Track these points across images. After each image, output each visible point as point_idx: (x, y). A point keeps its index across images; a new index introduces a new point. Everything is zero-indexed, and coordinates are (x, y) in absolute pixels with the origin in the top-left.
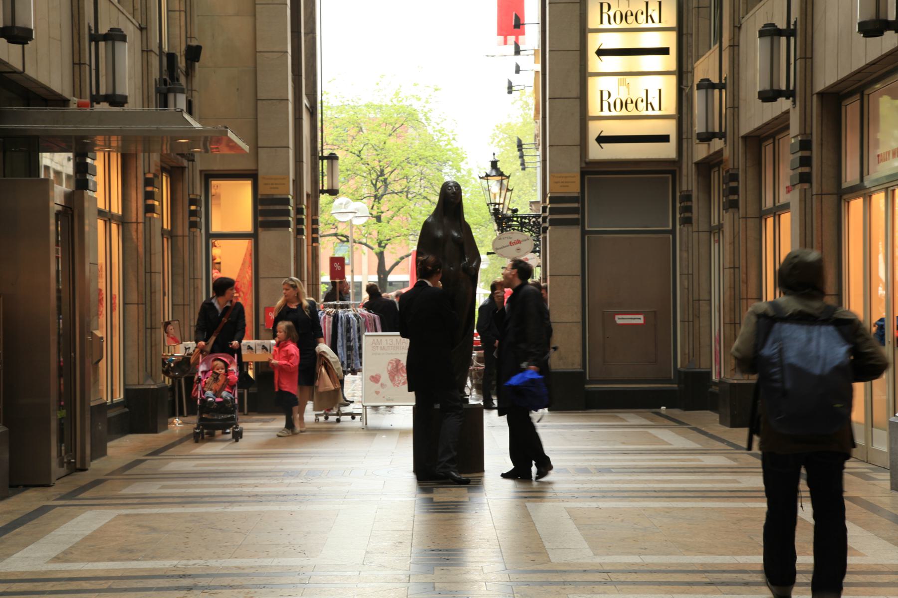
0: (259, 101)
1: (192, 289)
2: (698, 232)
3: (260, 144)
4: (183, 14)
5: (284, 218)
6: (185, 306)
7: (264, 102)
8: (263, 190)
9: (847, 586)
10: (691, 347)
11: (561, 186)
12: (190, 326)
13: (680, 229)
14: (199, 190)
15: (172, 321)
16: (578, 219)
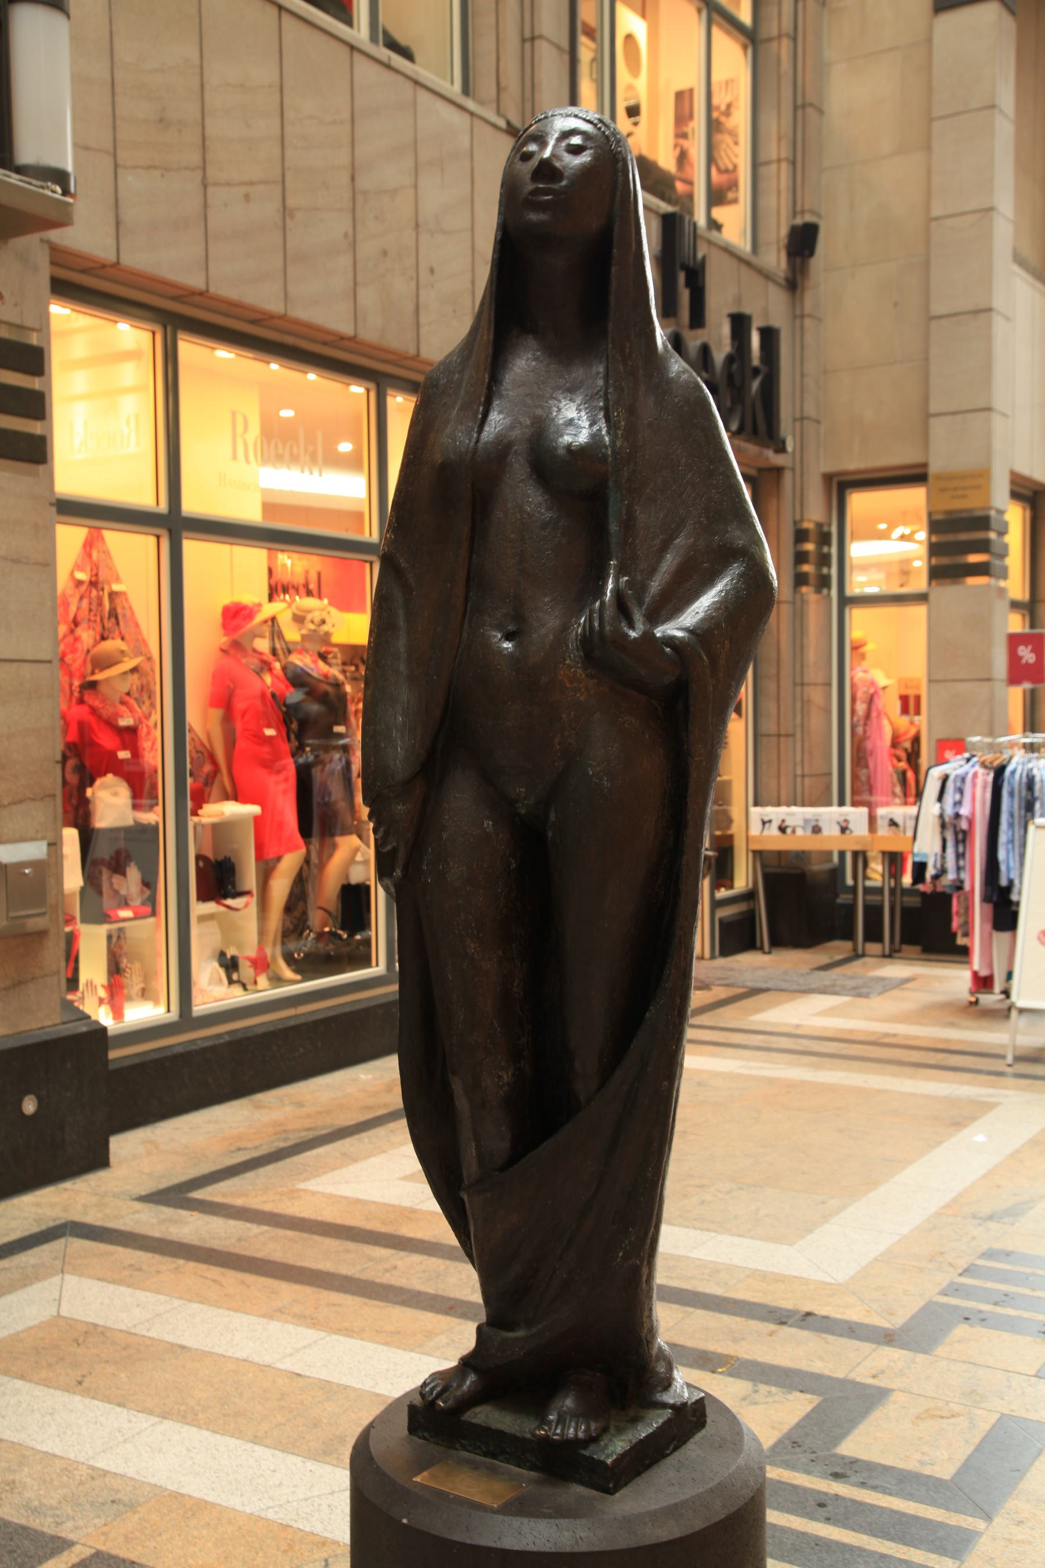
0: (934, 324)
1: (798, 705)
3: (933, 408)
4: (784, 166)
5: (979, 535)
6: (782, 739)
7: (943, 321)
12: (795, 776)
14: (815, 513)
15: (141, 654)
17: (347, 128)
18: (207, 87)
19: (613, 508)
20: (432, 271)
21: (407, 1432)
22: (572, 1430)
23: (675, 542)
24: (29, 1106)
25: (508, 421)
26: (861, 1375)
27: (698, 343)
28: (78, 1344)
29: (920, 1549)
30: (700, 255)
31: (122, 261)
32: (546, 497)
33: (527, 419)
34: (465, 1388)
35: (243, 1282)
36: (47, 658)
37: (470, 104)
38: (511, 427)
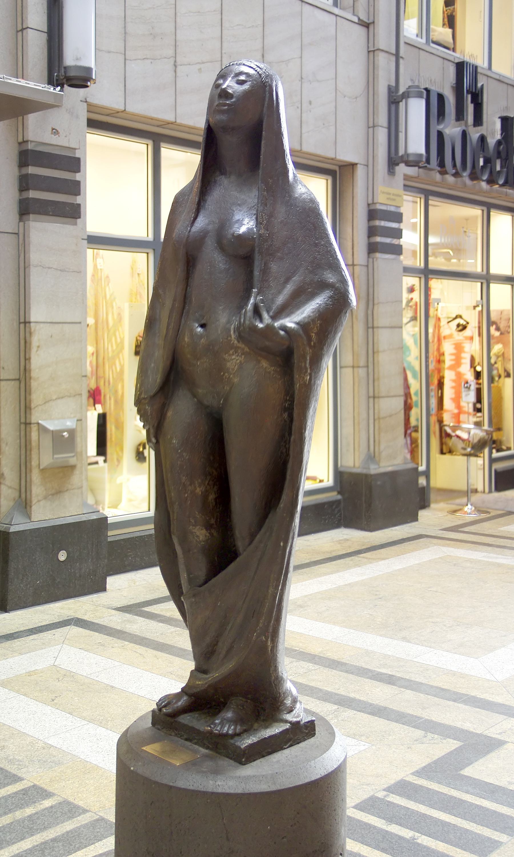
17: (261, 29)
18: (178, 14)
19: (257, 263)
20: (310, 103)
21: (151, 725)
22: (226, 729)
23: (293, 279)
24: (62, 556)
25: (207, 221)
26: (493, 733)
27: (478, 135)
28: (59, 681)
29: (490, 828)
30: (479, 85)
31: (126, 110)
32: (223, 258)
33: (217, 220)
34: (180, 703)
35: (156, 656)
36: (78, 321)
37: (336, 11)
38: (208, 225)
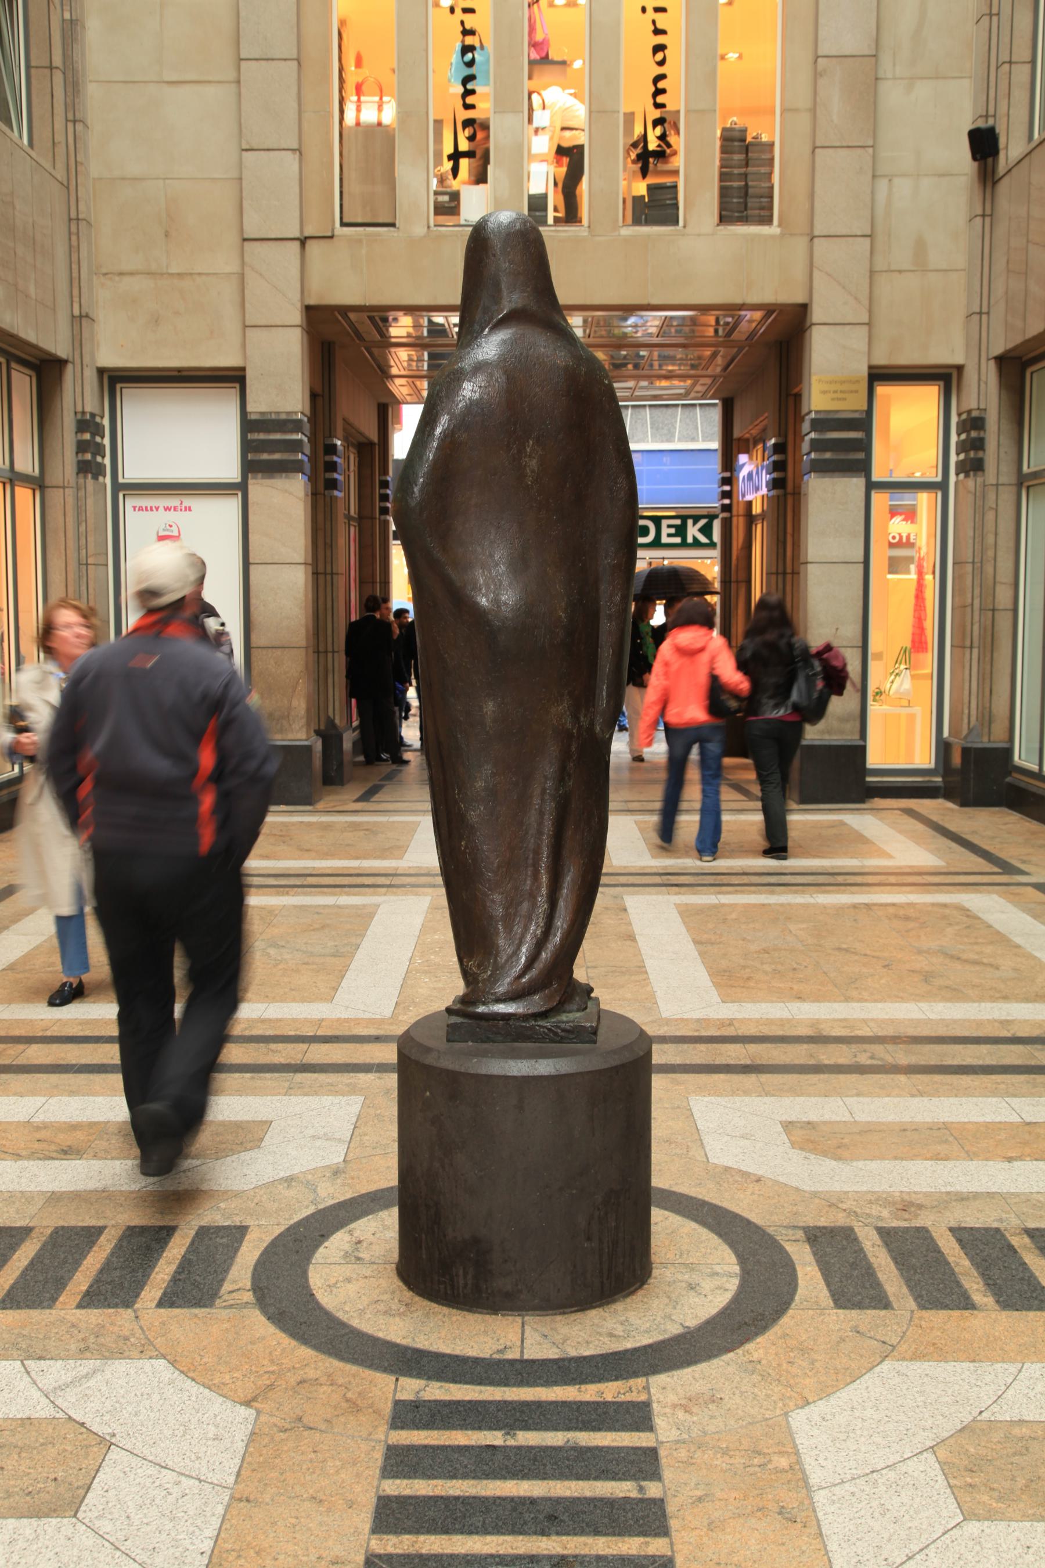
2: (997, 485)
8: (257, 406)
9: (658, 1072)
10: (330, 681)
11: (833, 399)
13: (956, 483)
16: (251, 431)
